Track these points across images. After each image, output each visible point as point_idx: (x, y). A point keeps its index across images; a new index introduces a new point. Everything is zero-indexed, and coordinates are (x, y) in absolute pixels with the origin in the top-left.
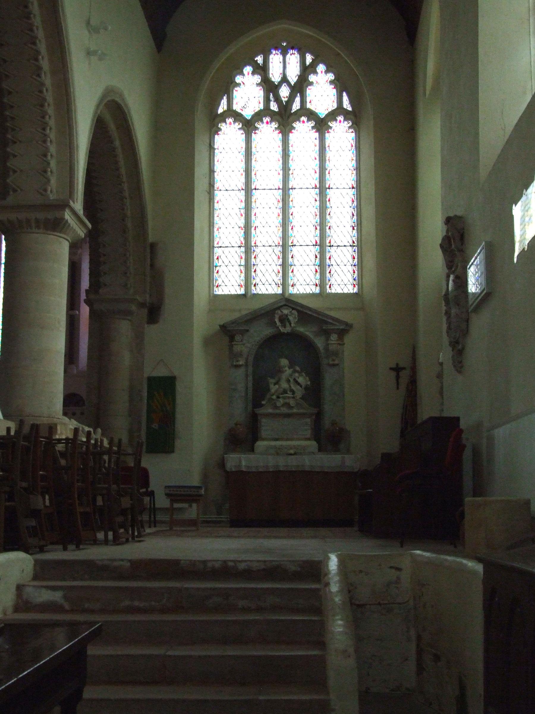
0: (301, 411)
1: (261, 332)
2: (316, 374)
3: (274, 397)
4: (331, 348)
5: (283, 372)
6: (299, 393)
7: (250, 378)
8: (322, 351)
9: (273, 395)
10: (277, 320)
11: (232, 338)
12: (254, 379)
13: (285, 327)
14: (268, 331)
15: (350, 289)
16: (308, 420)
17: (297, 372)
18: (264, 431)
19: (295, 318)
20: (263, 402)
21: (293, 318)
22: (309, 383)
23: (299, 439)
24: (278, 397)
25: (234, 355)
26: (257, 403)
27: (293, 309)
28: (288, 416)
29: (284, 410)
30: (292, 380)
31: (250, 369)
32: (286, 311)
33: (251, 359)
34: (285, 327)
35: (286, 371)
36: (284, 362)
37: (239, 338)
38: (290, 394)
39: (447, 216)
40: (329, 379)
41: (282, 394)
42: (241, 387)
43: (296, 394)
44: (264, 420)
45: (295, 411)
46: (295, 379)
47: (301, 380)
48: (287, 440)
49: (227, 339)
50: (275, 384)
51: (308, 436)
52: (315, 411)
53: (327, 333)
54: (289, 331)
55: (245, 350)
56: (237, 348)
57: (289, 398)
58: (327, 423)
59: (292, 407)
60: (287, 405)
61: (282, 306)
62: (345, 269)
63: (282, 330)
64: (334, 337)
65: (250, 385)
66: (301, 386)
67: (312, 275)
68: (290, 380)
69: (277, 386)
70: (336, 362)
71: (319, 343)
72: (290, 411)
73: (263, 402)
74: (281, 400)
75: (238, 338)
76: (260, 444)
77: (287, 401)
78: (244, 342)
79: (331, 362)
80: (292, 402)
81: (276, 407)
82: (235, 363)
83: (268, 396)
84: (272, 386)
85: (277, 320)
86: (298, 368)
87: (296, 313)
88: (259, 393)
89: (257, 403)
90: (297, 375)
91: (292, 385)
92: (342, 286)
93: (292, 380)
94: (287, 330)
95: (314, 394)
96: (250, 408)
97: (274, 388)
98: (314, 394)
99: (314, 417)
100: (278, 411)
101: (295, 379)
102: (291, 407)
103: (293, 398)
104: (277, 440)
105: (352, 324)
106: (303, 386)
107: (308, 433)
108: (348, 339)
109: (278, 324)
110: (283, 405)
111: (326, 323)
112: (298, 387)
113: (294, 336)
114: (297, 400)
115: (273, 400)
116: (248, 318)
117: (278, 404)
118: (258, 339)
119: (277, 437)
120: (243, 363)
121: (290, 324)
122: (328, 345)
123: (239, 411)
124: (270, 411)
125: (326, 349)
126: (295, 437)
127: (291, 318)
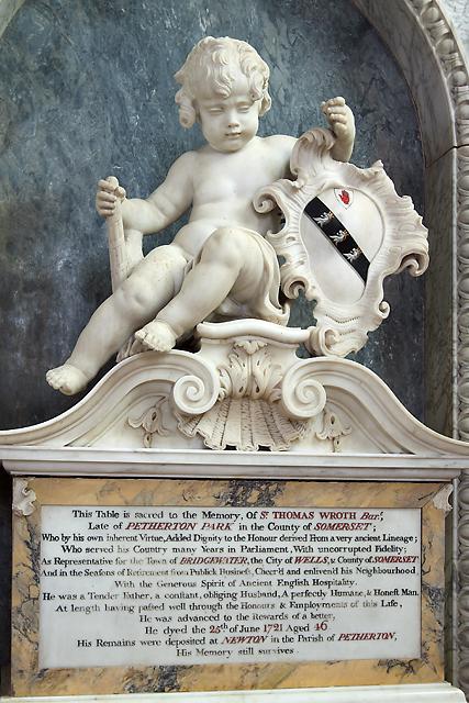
0: (354, 455)
3: (160, 335)
5: (230, 143)
6: (349, 310)
9: (151, 317)
16: (402, 523)
20: (65, 377)
24: (189, 342)
28: (244, 489)
29: (236, 446)
30: (294, 211)
38: (276, 323)
39: (118, 295)
41: (218, 317)
43: (324, 323)
44: (58, 521)
45: (308, 452)
51: (405, 646)
57: (272, 344)
59: (296, 422)
60: (260, 404)
66: (361, 265)
69: (171, 257)
73: (65, 377)
77: (264, 371)
80: (298, 386)
81: (163, 416)
84: (128, 250)
90: (330, 173)
91: (293, 252)
93: (294, 211)
97: (144, 274)
100: (172, 453)
101: (315, 209)
103: (307, 350)
105: (245, 221)
106: (379, 268)
110: (226, 402)
112: (341, 267)
114: (327, 369)
115: (150, 355)
119: (167, 657)
124: (116, 446)
126: (304, 651)
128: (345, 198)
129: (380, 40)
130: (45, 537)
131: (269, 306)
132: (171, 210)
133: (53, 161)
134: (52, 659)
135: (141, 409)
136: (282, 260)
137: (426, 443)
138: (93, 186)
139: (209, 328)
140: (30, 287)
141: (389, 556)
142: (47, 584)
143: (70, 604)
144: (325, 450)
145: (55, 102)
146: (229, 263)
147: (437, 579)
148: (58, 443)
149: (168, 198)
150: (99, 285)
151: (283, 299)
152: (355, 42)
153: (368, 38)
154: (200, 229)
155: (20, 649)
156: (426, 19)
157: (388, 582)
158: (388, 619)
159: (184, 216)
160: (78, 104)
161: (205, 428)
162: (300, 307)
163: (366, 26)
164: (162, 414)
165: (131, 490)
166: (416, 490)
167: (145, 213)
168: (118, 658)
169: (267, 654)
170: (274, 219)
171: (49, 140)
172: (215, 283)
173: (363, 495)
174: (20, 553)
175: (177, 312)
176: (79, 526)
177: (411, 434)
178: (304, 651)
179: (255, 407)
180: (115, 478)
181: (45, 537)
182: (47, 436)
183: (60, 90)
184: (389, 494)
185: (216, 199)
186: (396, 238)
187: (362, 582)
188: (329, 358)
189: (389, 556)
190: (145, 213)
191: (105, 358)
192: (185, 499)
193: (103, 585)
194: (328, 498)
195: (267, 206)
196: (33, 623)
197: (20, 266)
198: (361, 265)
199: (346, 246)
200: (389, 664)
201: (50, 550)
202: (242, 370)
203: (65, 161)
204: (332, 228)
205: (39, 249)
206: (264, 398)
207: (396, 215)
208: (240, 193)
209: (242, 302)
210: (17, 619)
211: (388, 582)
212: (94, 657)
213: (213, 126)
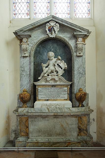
0: (62, 83)
1: (38, 36)
2: (69, 61)
3: (46, 75)
4: (78, 46)
5: (51, 60)
6: (61, 72)
7: (32, 64)
8: (73, 48)
10: (47, 30)
11: (21, 41)
12: (34, 64)
13: (52, 34)
14: (42, 37)
15: (85, 16)
16: (66, 88)
17: (60, 60)
18: (39, 96)
19: (58, 28)
20: (39, 78)
21: (57, 28)
22: (66, 66)
23: (61, 100)
24: (48, 75)
25: (22, 50)
26: (36, 79)
27: (57, 22)
28: (53, 86)
29: (52, 83)
30: (56, 65)
31: (32, 58)
32: (52, 24)
33: (33, 53)
34: (52, 34)
35: (52, 59)
36: (51, 54)
37: (25, 40)
40: (77, 63)
41: (50, 73)
42: (27, 69)
43: (59, 73)
44: (39, 89)
46: (58, 64)
47: (61, 65)
48: (54, 100)
49: (19, 42)
50: (46, 67)
51: (66, 98)
52: (70, 83)
53: (75, 37)
54: (54, 37)
55: (29, 48)
56: (24, 46)
57: (54, 75)
58: (76, 89)
60: (54, 80)
61: (50, 21)
62: (84, 5)
63: (51, 36)
64: (80, 40)
65: (32, 67)
66: (62, 68)
67: (66, 8)
68: (54, 64)
69: (47, 68)
70: (81, 54)
71: (72, 43)
72: (55, 84)
73: (39, 78)
74: (50, 76)
75: (25, 40)
76: (38, 104)
77: (54, 77)
78: (28, 43)
79: (78, 55)
80: (57, 78)
81: (47, 81)
82: (23, 55)
83: (42, 74)
84: (44, 68)
85: (47, 30)
86: (60, 58)
87: (58, 25)
88: (37, 73)
89: (36, 80)
90: (59, 61)
92: (82, 15)
93: (56, 65)
94: (53, 36)
95: (69, 73)
96: (32, 82)
97: (45, 70)
98: (69, 73)
99: (69, 87)
100: (47, 83)
101: (58, 64)
102: (55, 81)
103: (57, 75)
104: (48, 100)
107: (66, 96)
108: (87, 41)
109: (48, 32)
110: (51, 80)
111: (75, 30)
113: (57, 40)
116: (31, 27)
117: (48, 79)
118: (36, 41)
120: (28, 55)
121: (55, 32)
122: (77, 44)
123: (27, 85)
124: (43, 83)
125: (76, 47)
126: (58, 98)
127: (55, 28)
128: (60, 63)
129: (67, 46)
130: (95, 133)
131: (54, 72)
132: (48, 65)
133: (40, 60)
134: (39, 99)
135: (45, 80)
136: (55, 68)
137: (67, 82)
138: (41, 64)
139: (49, 74)
140: (38, 70)
141: (65, 91)
142: (39, 93)
143: (40, 95)
144: (59, 83)
145: (40, 55)
146: (50, 70)
147: (69, 93)
148: (39, 83)
149: (47, 64)
150: (43, 71)
151: (56, 71)
152: (65, 47)
153: (66, 46)
154: (49, 66)
155: (37, 98)
156: (70, 46)
157: (65, 93)
158: (65, 96)
159: (49, 65)
160: (42, 55)
161: (50, 81)
162: (57, 72)
163: (66, 45)
164: (47, 81)
165: (45, 86)
166: (67, 86)
167: (45, 65)
168: (44, 98)
169: (55, 98)
170: (55, 65)
171: (39, 58)
172: (50, 71)
173: (63, 86)
174: (37, 91)
175: (47, 73)
176: (41, 89)
177: (66, 81)
178: (58, 98)
179: (54, 80)
180: (43, 85)
181: (95, 133)
182: (38, 82)
183: (40, 54)
184: (65, 86)
185: (51, 64)
186: (64, 66)
187: (63, 93)
188: (59, 76)
189: (65, 91)
190: (45, 65)
191: (42, 77)
192: (49, 87)
193: (43, 93)
194: (60, 87)
195: (54, 64)
196: (38, 96)
197: (37, 69)
198: (62, 68)
199: (60, 67)
200: (65, 99)
201: (39, 91)
202: (52, 77)
203: (41, 60)
204: (59, 66)
205: (39, 67)
206: (54, 79)
207: (64, 64)
208: (52, 63)
209: (52, 72)
210: (37, 96)
211: (65, 93)
212: (42, 98)
213: (50, 59)
